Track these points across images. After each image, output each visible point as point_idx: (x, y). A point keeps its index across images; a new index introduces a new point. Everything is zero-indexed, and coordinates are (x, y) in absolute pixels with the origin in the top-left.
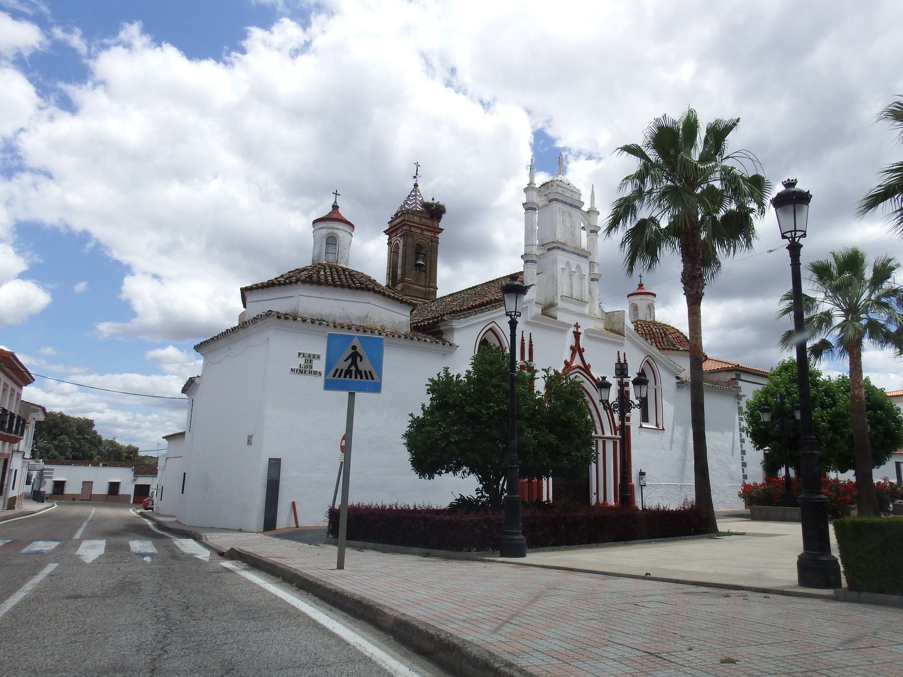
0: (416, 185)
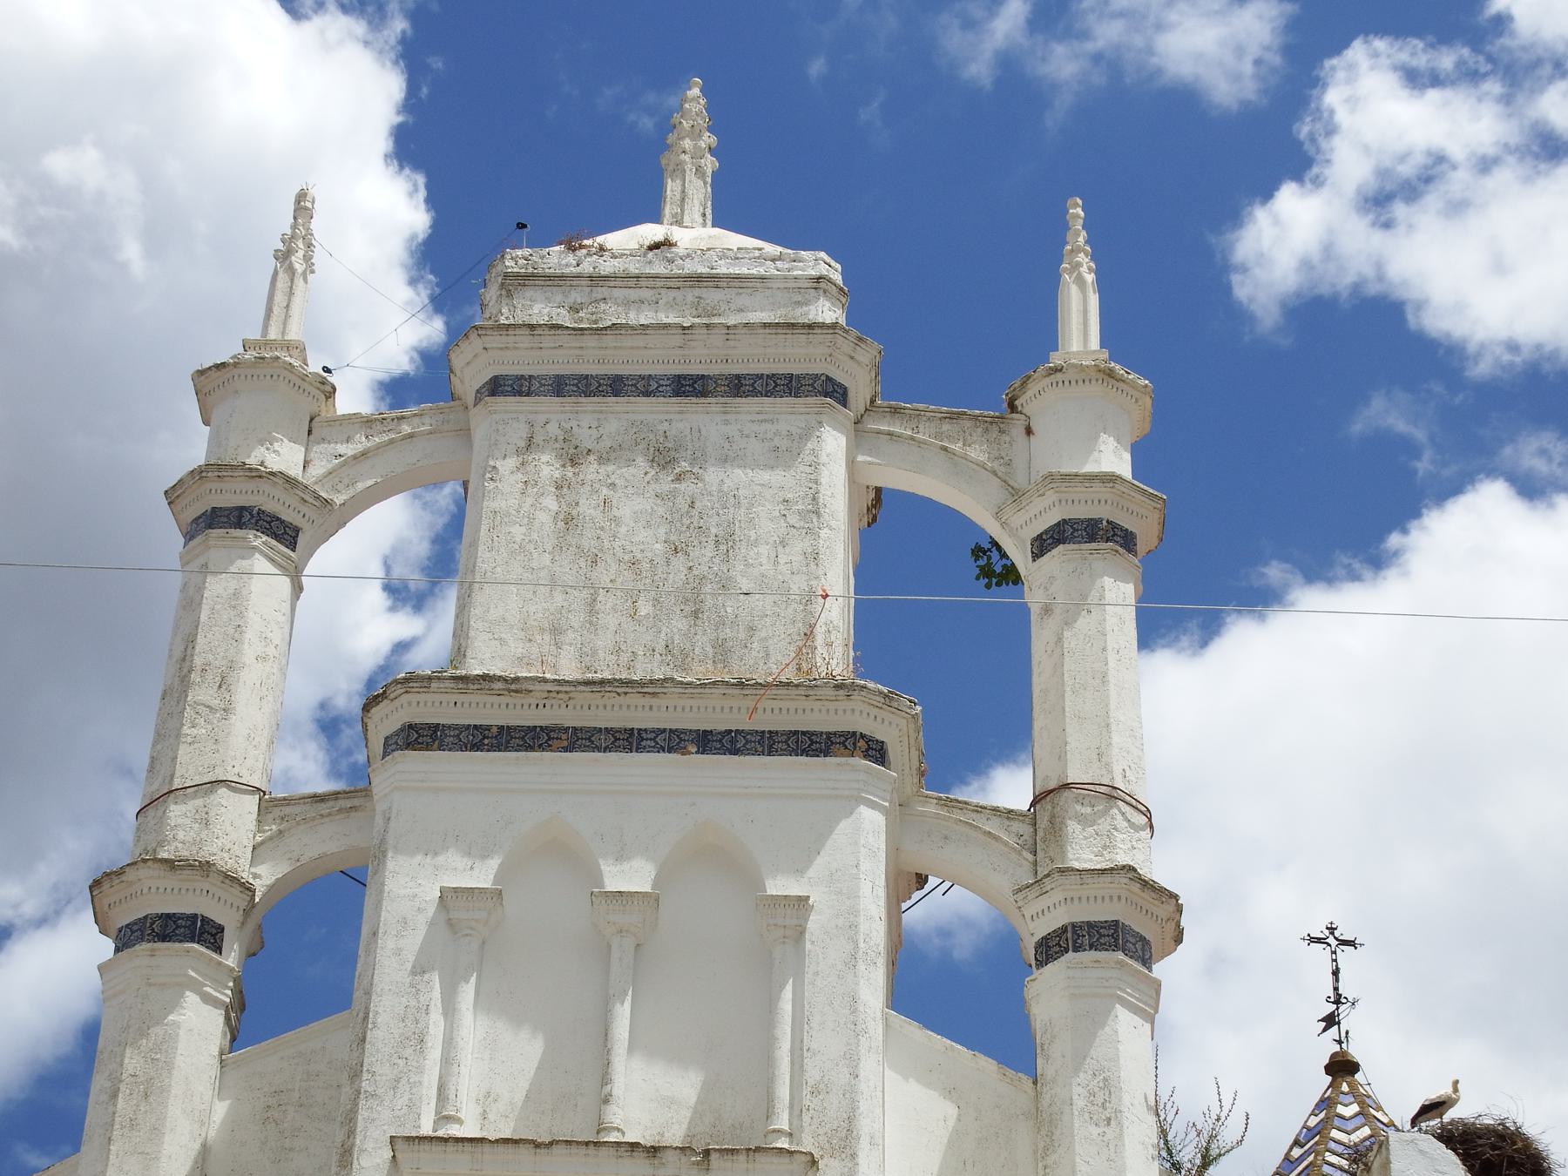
0: (1341, 1067)
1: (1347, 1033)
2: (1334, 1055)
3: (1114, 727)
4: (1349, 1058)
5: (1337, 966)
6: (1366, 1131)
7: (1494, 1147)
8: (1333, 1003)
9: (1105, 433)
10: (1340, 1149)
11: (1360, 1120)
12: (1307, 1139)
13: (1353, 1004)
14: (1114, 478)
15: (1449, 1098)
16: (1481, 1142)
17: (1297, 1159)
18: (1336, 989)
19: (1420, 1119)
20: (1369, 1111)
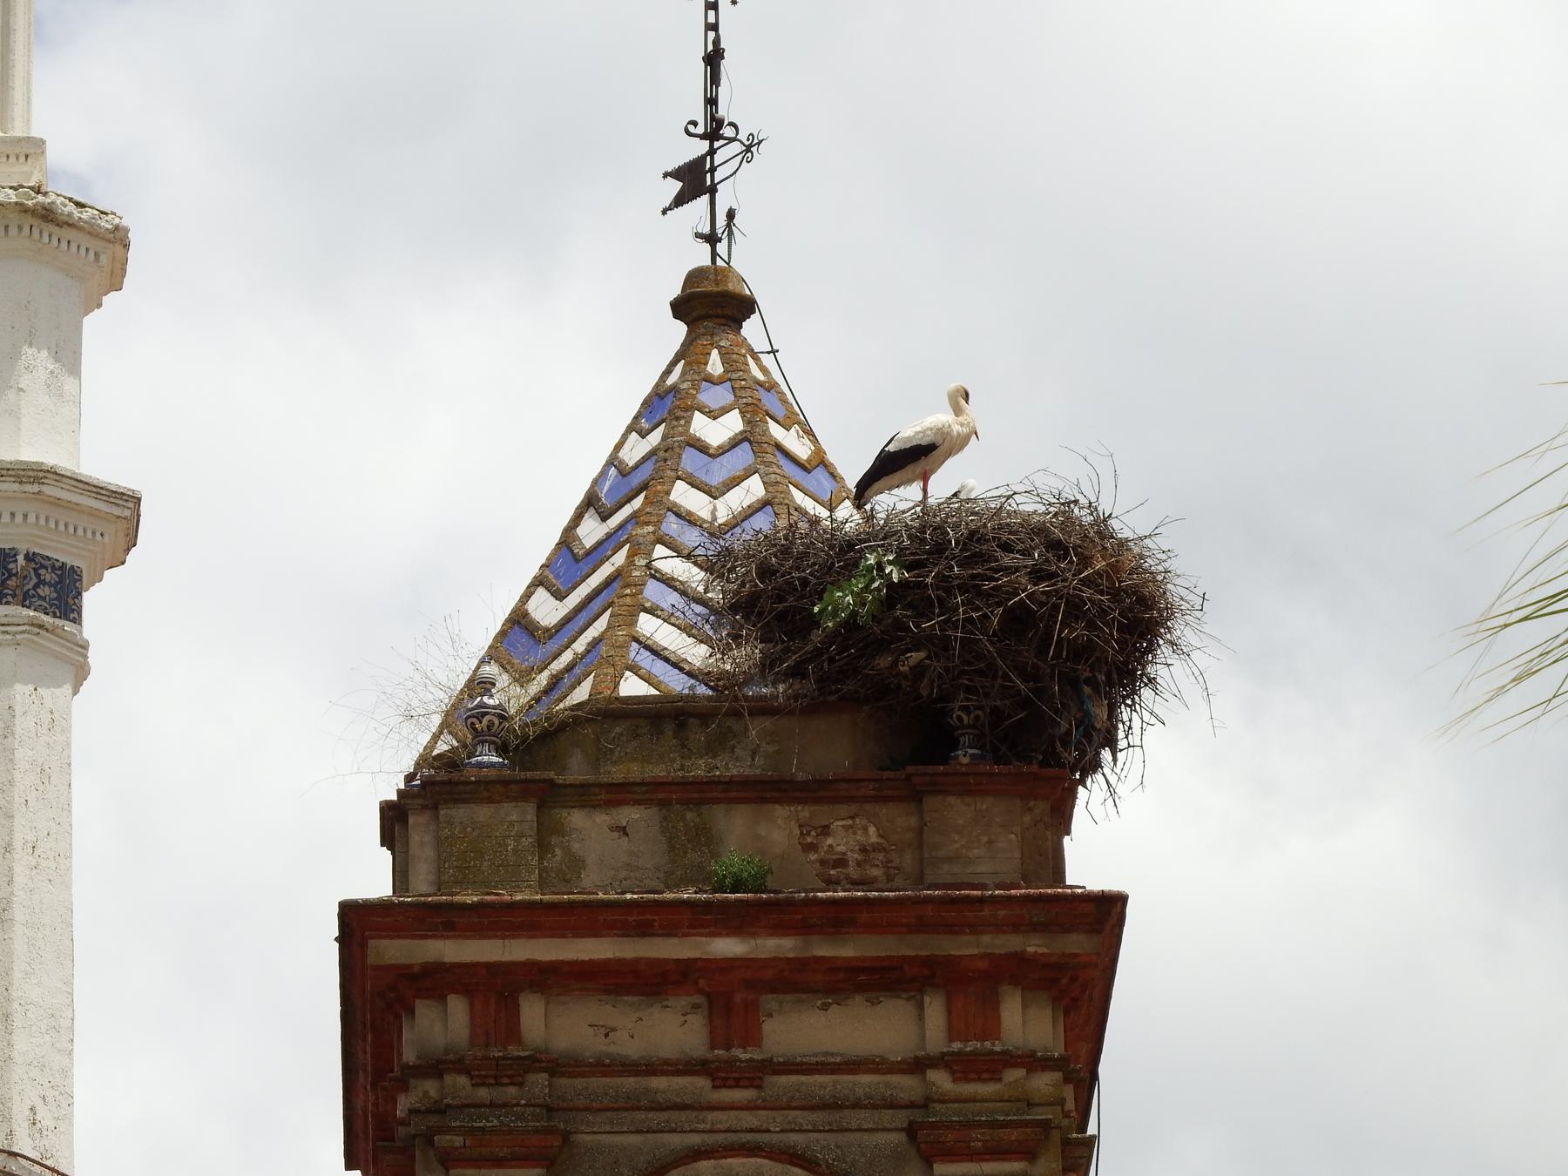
1: (731, 215)
2: (695, 277)
3: (18, 1021)
4: (731, 287)
5: (717, 42)
6: (753, 489)
7: (1038, 575)
8: (702, 137)
9: (31, 345)
10: (691, 538)
11: (743, 457)
12: (619, 496)
13: (748, 149)
14: (42, 474)
15: (943, 432)
16: (1007, 560)
17: (589, 553)
18: (711, 102)
19: (877, 486)
20: (766, 431)
